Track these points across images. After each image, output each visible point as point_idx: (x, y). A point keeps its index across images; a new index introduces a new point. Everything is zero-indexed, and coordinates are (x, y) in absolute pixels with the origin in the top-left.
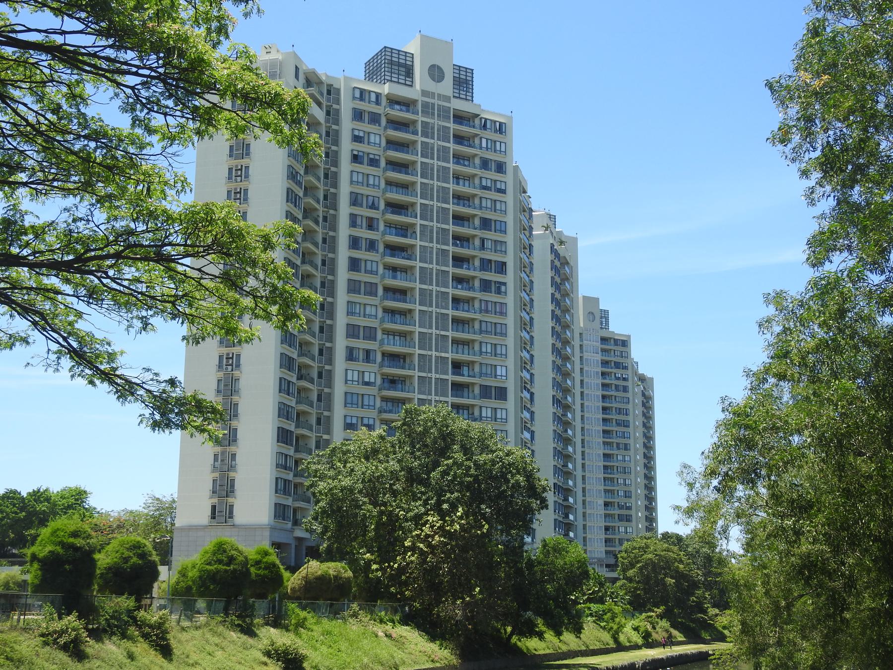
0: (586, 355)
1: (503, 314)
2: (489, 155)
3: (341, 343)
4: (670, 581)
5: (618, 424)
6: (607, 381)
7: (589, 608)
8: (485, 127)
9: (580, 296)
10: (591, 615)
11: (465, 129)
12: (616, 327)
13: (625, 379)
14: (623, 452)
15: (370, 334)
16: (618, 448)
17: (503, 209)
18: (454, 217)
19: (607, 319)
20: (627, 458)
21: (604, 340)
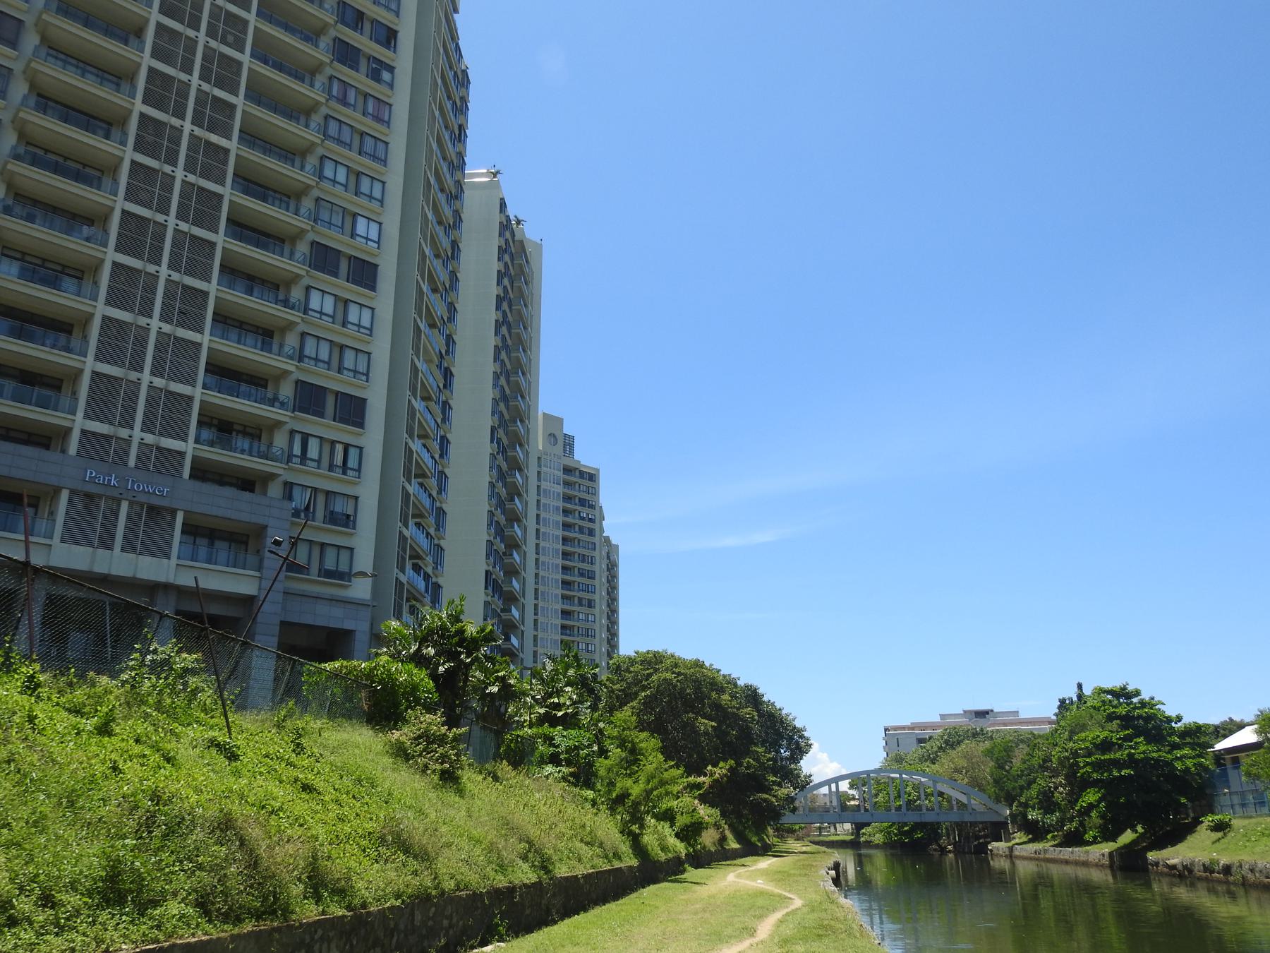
0: (544, 485)
1: (347, 521)
2: (334, 239)
4: (705, 724)
6: (570, 520)
7: (549, 740)
9: (540, 414)
10: (555, 760)
12: (584, 456)
13: (591, 521)
14: (586, 609)
16: (581, 605)
17: (366, 322)
18: (212, 368)
21: (568, 470)
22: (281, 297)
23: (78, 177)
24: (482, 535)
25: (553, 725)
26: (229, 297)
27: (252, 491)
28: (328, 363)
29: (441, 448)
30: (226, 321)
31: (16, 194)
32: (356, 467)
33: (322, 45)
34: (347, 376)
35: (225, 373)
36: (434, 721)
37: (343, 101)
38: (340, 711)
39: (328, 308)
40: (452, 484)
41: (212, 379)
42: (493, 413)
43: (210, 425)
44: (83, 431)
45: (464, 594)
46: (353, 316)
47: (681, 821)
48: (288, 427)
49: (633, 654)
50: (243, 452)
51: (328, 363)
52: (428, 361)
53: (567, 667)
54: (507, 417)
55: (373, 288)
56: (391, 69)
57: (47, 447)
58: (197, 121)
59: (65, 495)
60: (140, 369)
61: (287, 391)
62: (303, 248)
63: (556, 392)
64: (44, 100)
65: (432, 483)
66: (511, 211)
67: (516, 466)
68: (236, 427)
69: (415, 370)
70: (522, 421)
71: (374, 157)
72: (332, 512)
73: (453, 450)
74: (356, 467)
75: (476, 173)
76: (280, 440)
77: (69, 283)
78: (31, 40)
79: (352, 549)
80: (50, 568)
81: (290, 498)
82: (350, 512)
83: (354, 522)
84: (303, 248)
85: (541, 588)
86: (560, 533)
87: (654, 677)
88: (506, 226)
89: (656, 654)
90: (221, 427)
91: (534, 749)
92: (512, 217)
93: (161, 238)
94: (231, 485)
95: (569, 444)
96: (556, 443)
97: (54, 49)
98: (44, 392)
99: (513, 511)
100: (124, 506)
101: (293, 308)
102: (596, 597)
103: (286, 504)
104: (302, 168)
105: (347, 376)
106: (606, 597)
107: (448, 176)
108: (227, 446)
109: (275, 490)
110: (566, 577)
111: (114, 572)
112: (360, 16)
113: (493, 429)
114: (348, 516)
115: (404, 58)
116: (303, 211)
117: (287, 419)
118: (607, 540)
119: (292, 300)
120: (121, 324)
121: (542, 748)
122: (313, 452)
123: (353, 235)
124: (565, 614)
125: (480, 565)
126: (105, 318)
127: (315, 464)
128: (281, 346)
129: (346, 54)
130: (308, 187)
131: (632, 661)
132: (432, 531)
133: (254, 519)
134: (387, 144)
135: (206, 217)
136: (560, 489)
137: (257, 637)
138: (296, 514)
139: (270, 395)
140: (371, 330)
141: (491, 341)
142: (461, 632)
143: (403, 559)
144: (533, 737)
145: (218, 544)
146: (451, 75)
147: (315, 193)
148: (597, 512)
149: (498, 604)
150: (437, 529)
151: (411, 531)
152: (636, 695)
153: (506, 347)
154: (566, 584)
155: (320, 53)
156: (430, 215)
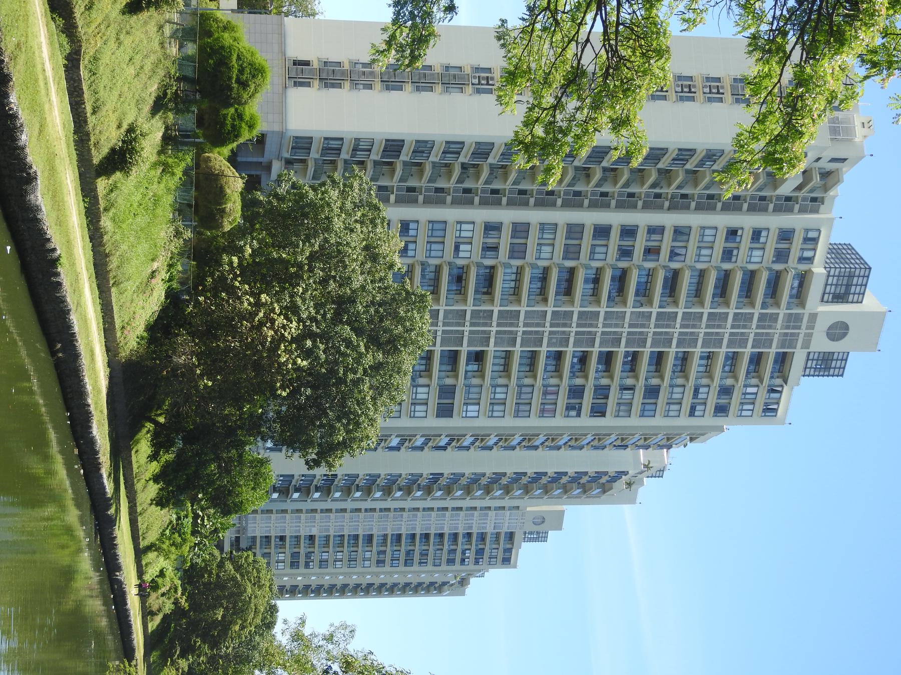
0: (492, 514)
3: (506, 216)
4: (219, 614)
7: (186, 516)
9: (564, 507)
10: (179, 518)
13: (463, 561)
14: (375, 558)
16: (379, 553)
19: (536, 540)
20: (367, 563)
21: (511, 536)
25: (193, 518)
47: (160, 581)
85: (391, 514)
86: (461, 531)
95: (540, 537)
110: (404, 538)
121: (182, 514)
144: (187, 511)
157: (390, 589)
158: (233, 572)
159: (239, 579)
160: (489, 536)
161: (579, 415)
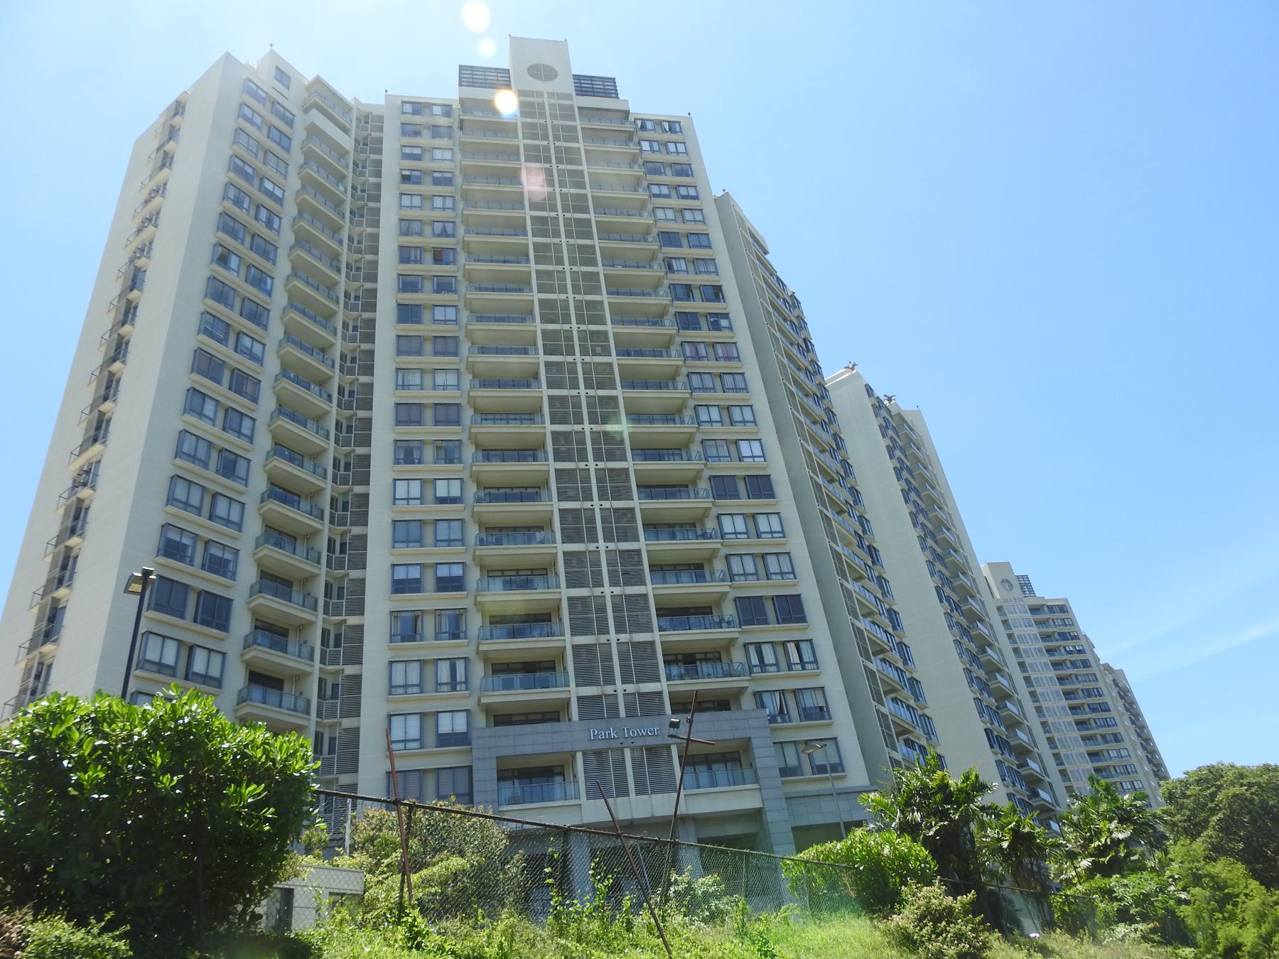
0: (1016, 632)
1: (821, 713)
2: (726, 468)
3: (383, 435)
5: (1093, 709)
6: (1057, 658)
7: (1108, 893)
8: (643, 128)
9: (983, 566)
10: (1124, 916)
11: (696, 635)
12: (1046, 591)
13: (1079, 652)
15: (448, 414)
16: (1106, 742)
17: (776, 527)
18: (662, 612)
19: (1029, 585)
20: (1123, 753)
21: (1035, 610)
22: (699, 533)
23: (522, 498)
24: (967, 694)
26: (658, 548)
27: (729, 709)
28: (756, 574)
29: (892, 621)
30: (661, 568)
31: (487, 529)
32: (812, 659)
33: (667, 322)
34: (776, 580)
35: (674, 613)
36: (934, 894)
37: (697, 357)
38: (819, 903)
39: (741, 527)
40: (914, 652)
41: (665, 621)
42: (932, 574)
43: (676, 662)
44: (579, 698)
45: (965, 753)
46: (763, 527)
48: (740, 642)
49: (1183, 776)
50: (709, 676)
51: (756, 574)
52: (849, 544)
53: (1096, 802)
54: (947, 574)
55: (772, 496)
56: (726, 316)
57: (558, 720)
58: (593, 421)
59: (579, 757)
60: (605, 631)
61: (729, 610)
62: (704, 485)
63: (989, 540)
64: (488, 452)
65: (895, 656)
66: (880, 392)
67: (975, 618)
68: (698, 656)
69: (837, 556)
70: (963, 573)
71: (736, 389)
72: (805, 709)
73: (904, 619)
74: (812, 659)
75: (832, 372)
76: (738, 656)
77: (538, 580)
78: (468, 414)
79: (835, 739)
80: (587, 825)
81: (762, 705)
82: (821, 703)
83: (828, 711)
84: (704, 485)
87: (1220, 796)
88: (878, 406)
89: (1210, 769)
90: (685, 660)
91: (1094, 908)
92: (882, 398)
93: (591, 520)
94: (709, 709)
96: (1011, 587)
97: (485, 414)
98: (544, 674)
99: (990, 662)
100: (627, 753)
101: (711, 538)
102: (1120, 729)
103: (760, 712)
104: (682, 422)
105: (776, 580)
106: (1132, 727)
107: (807, 381)
108: (695, 674)
109: (748, 702)
111: (636, 816)
112: (688, 288)
113: (938, 590)
114: (821, 708)
115: (733, 304)
116: (694, 455)
117: (737, 635)
118: (1107, 668)
119: (709, 531)
120: (583, 600)
122: (769, 657)
123: (741, 459)
124: (1093, 755)
125: (976, 726)
126: (570, 599)
127: (774, 668)
128: (712, 573)
129: (688, 321)
130: (692, 434)
131: (1185, 784)
132: (912, 703)
133: (738, 735)
134: (742, 374)
135: (621, 492)
136: (1035, 630)
137: (775, 848)
138: (773, 719)
139: (717, 620)
140: (783, 532)
141: (905, 510)
142: (943, 787)
143: (891, 736)
144: (1087, 894)
145: (715, 767)
146: (780, 302)
147: (699, 437)
148: (1083, 641)
149: (1011, 761)
150: (917, 699)
151: (888, 707)
152: (1206, 821)
153: (922, 511)
154: (1080, 724)
155: (669, 328)
156: (802, 418)
157: (1146, 742)
158: (1210, 832)
159: (1220, 815)
160: (1042, 630)
161: (726, 316)
